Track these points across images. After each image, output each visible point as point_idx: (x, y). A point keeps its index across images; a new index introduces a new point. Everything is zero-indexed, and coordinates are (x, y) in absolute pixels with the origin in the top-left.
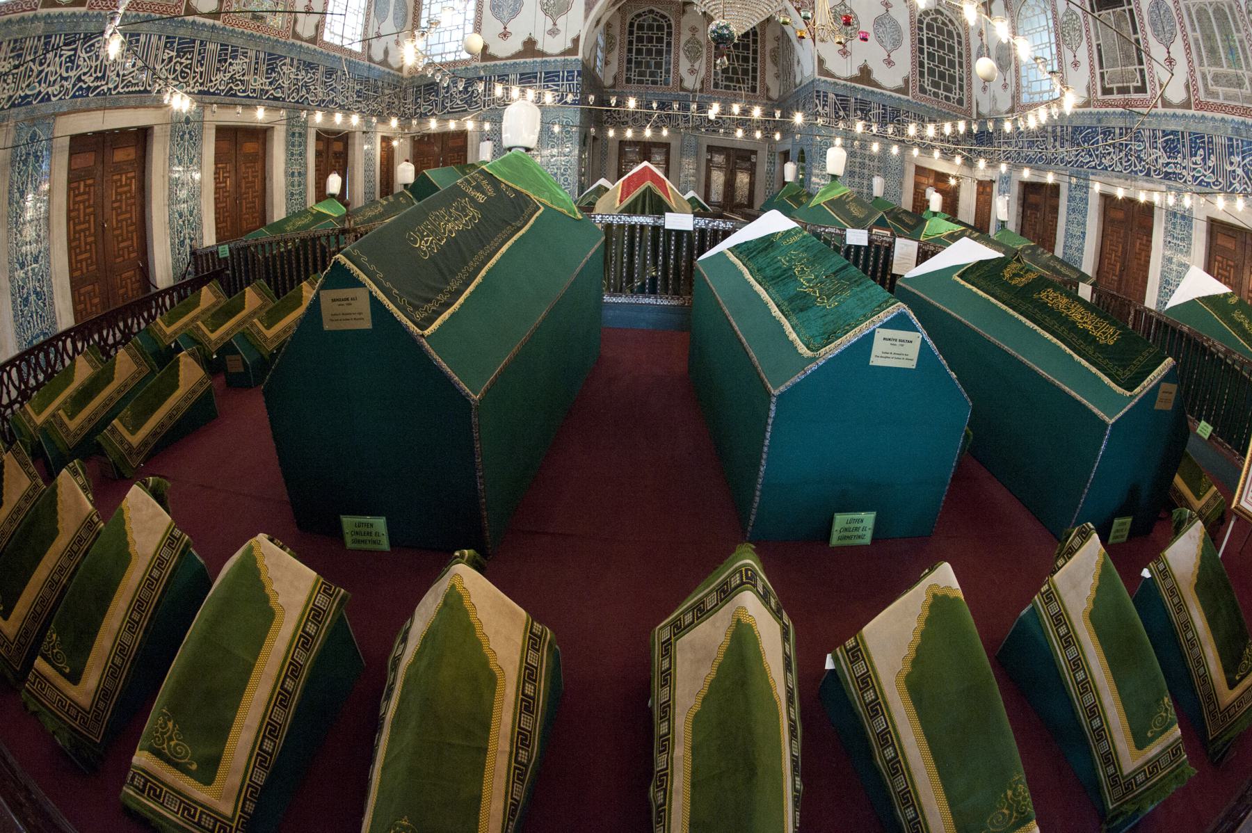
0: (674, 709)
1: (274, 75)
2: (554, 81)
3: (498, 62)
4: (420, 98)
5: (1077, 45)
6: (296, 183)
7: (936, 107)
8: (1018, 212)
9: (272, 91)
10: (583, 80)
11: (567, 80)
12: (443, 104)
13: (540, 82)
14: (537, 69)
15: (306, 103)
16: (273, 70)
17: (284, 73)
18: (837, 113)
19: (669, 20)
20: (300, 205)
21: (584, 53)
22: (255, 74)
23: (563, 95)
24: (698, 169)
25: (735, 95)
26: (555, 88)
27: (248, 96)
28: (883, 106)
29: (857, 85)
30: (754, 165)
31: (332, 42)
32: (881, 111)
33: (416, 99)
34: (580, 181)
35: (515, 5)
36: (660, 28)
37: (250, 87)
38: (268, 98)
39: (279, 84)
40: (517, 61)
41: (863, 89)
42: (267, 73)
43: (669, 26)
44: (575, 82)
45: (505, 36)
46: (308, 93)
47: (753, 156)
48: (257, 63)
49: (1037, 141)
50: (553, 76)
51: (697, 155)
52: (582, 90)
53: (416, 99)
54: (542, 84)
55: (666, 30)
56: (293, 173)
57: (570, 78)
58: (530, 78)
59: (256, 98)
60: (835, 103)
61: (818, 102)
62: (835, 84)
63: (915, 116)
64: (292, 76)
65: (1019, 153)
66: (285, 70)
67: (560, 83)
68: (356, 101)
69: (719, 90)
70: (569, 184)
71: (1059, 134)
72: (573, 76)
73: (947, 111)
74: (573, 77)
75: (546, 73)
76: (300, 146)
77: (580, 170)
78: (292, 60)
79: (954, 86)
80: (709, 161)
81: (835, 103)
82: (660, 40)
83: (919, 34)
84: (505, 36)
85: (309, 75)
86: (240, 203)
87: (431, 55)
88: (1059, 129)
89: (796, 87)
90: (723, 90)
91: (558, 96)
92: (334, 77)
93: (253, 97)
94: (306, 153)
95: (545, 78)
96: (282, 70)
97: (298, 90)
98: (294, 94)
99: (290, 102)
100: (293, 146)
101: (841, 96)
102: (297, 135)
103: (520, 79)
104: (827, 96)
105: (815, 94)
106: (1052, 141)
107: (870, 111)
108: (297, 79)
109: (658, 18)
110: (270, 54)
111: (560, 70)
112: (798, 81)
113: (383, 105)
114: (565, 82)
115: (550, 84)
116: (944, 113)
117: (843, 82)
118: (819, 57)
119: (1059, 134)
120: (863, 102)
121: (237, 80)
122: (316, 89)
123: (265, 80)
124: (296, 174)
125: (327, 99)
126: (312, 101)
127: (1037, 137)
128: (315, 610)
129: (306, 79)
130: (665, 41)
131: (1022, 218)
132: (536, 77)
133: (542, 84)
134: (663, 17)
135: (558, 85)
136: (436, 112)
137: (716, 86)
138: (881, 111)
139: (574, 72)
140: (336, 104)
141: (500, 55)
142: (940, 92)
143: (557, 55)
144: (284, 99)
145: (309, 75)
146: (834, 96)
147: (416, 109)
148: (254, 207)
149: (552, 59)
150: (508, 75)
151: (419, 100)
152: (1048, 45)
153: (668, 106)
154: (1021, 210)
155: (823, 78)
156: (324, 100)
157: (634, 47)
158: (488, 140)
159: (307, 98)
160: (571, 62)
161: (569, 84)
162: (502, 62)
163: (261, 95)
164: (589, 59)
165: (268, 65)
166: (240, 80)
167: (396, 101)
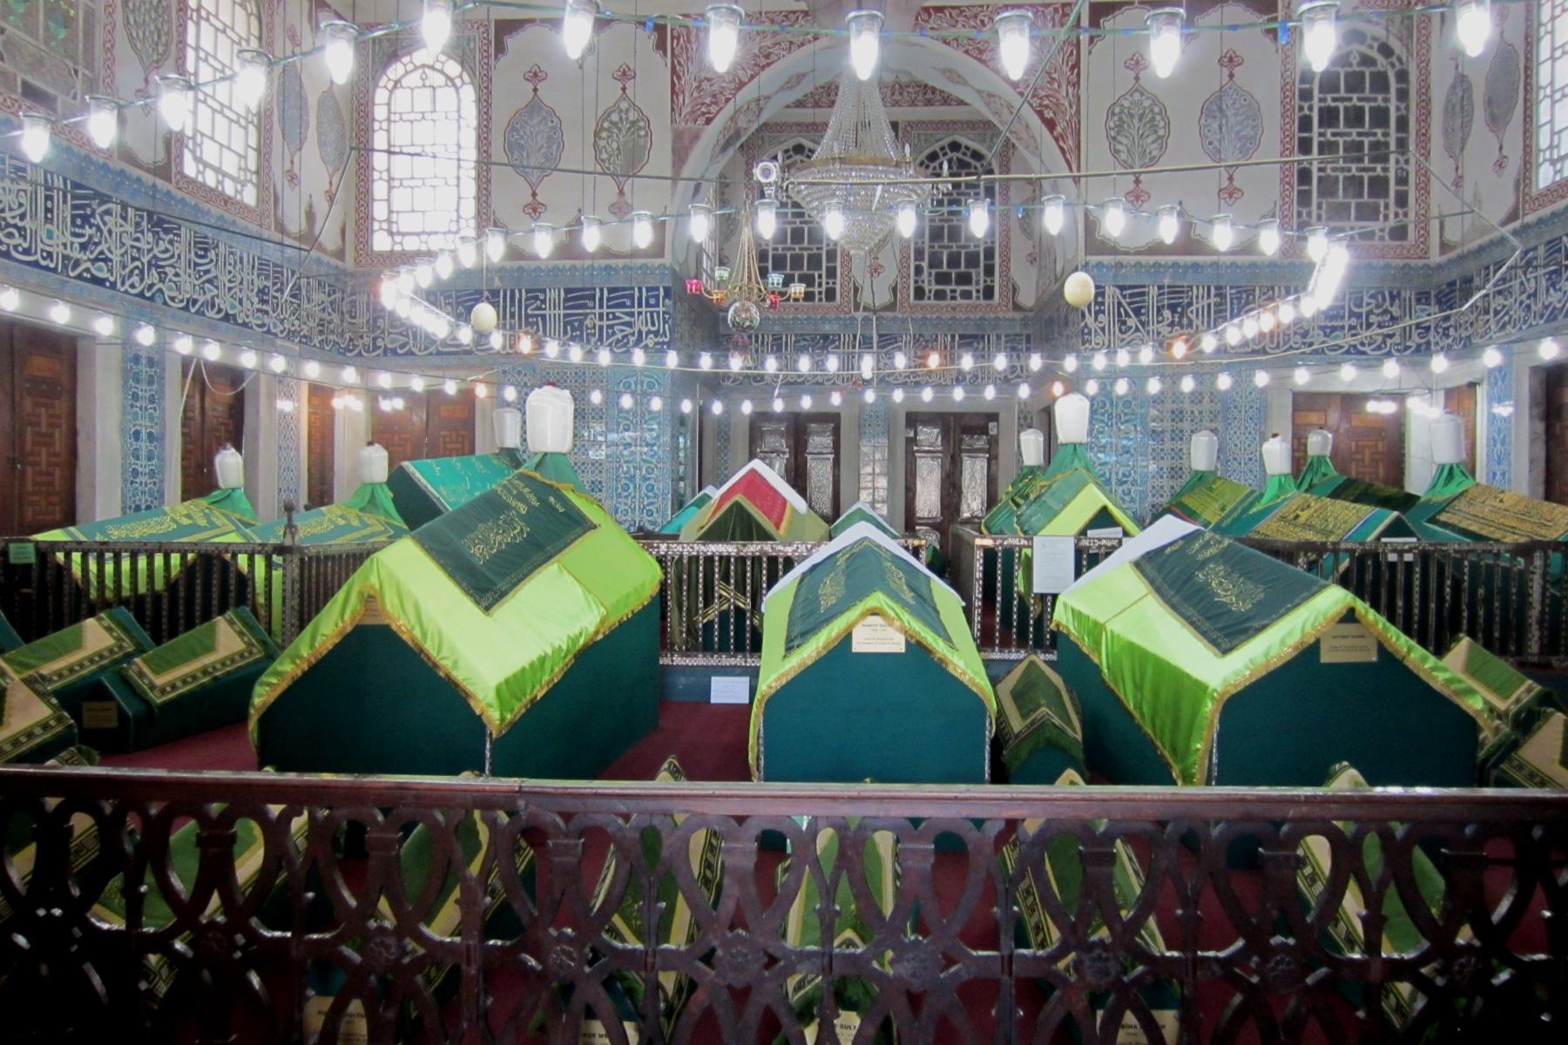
1: (88, 231)
2: (623, 305)
6: (143, 454)
8: (1533, 432)
9: (88, 265)
10: (675, 303)
11: (648, 305)
13: (601, 307)
15: (159, 301)
16: (86, 219)
17: (110, 232)
20: (151, 495)
21: (673, 252)
22: (48, 220)
24: (891, 458)
25: (954, 309)
26: (627, 319)
27: (36, 264)
30: (993, 442)
34: (675, 491)
35: (549, 147)
37: (40, 246)
38: (79, 277)
39: (102, 253)
42: (74, 224)
44: (661, 309)
45: (535, 210)
46: (162, 281)
47: (991, 425)
48: (48, 198)
50: (623, 297)
51: (890, 434)
52: (674, 323)
54: (605, 310)
56: (137, 435)
57: (652, 301)
58: (581, 298)
59: (54, 270)
64: (128, 242)
65: (1529, 307)
66: (111, 224)
67: (636, 310)
68: (259, 310)
69: (925, 302)
70: (656, 496)
72: (657, 297)
74: (658, 300)
75: (611, 291)
76: (151, 382)
77: (675, 471)
78: (124, 207)
79: (1382, 202)
80: (911, 442)
83: (1301, 109)
85: (162, 246)
86: (23, 472)
87: (399, 233)
90: (933, 302)
92: (212, 254)
93: (47, 268)
94: (162, 397)
95: (609, 300)
96: (105, 223)
97: (142, 272)
98: (135, 279)
99: (126, 292)
100: (138, 381)
102: (144, 361)
103: (566, 300)
107: (1190, 304)
108: (139, 249)
110: (76, 186)
111: (634, 284)
113: (312, 324)
115: (618, 312)
120: (1175, 291)
121: (8, 225)
122: (177, 275)
124: (144, 436)
125: (202, 299)
126: (172, 299)
129: (156, 251)
131: (1548, 442)
132: (593, 298)
133: (605, 310)
135: (632, 315)
137: (920, 293)
139: (657, 289)
140: (220, 311)
144: (113, 286)
145: (162, 246)
148: (52, 484)
150: (544, 291)
153: (833, 342)
154: (1540, 427)
156: (195, 302)
159: (160, 290)
161: (652, 313)
163: (65, 267)
164: (686, 260)
165: (75, 207)
166: (15, 226)
167: (335, 317)
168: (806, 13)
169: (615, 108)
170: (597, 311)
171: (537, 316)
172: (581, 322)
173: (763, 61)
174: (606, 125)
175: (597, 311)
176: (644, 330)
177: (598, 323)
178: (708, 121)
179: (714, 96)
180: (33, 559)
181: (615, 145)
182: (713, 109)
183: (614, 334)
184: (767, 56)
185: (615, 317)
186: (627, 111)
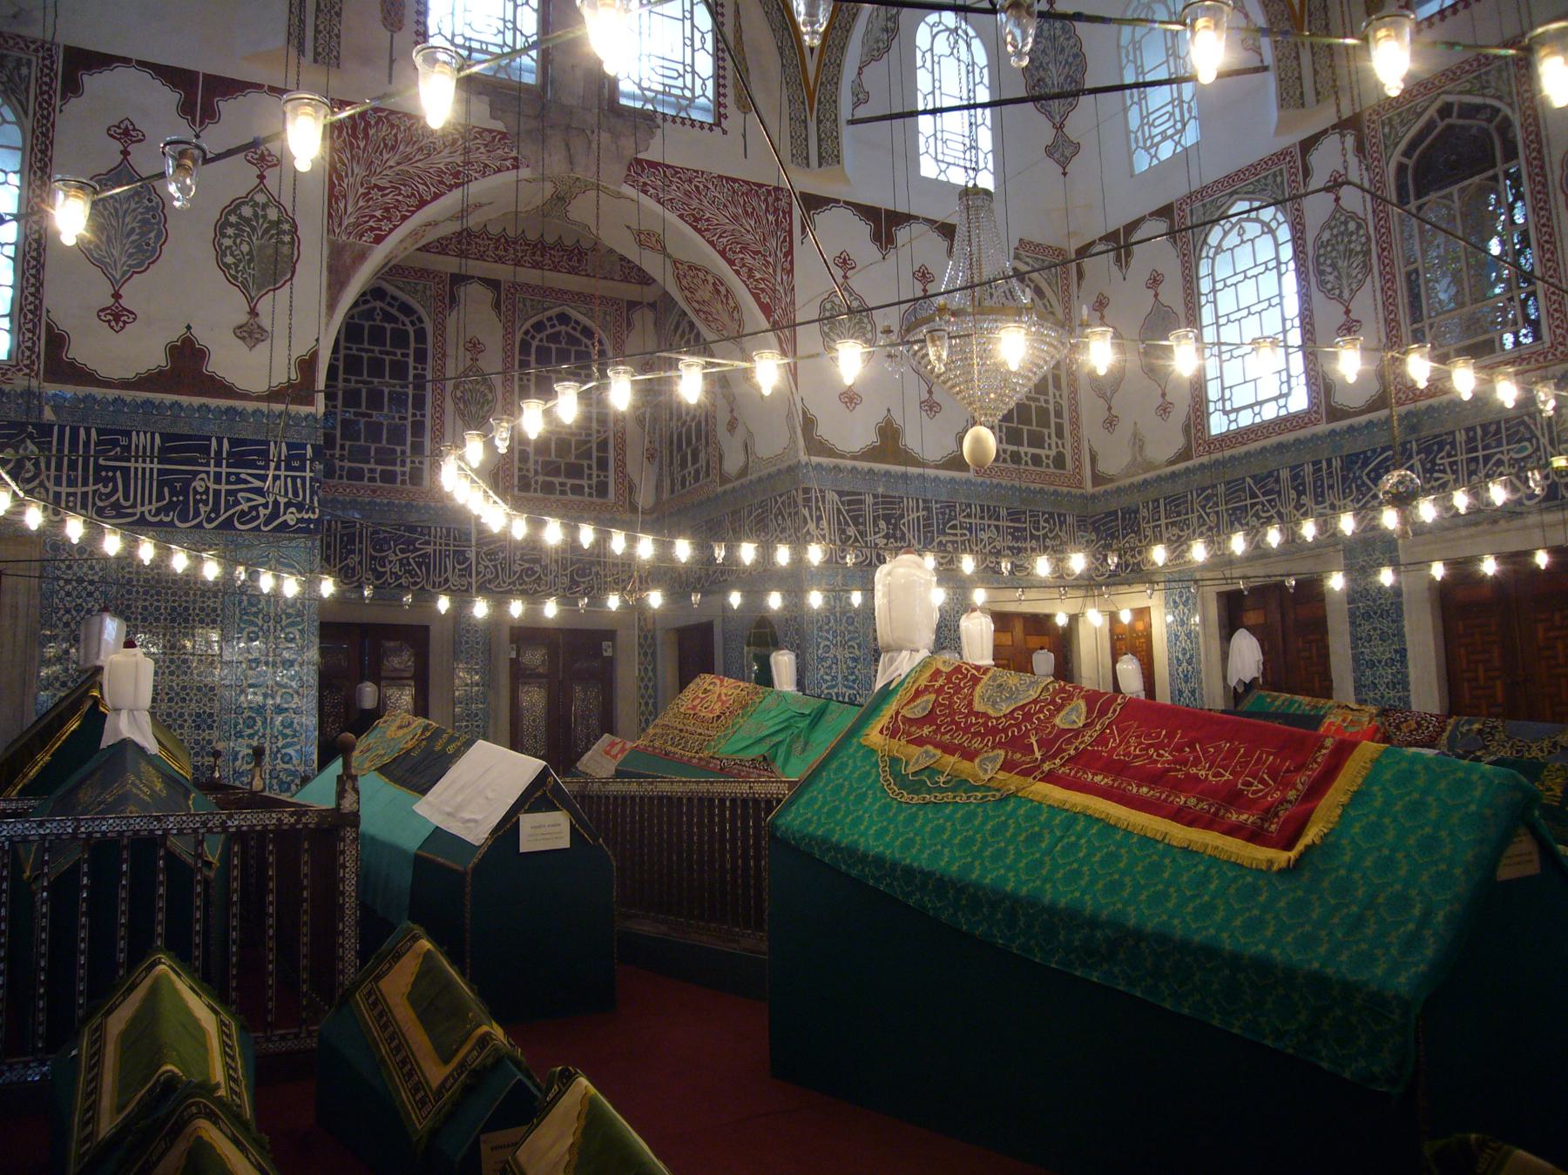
2: (253, 465)
3: (98, 392)
5: (1354, 286)
7: (1017, 483)
13: (218, 464)
14: (211, 428)
18: (843, 532)
19: (420, 320)
23: (276, 503)
26: (257, 484)
28: (925, 501)
29: (877, 466)
32: (921, 513)
36: (400, 339)
40: (157, 397)
41: (887, 473)
43: (421, 335)
44: (308, 474)
49: (1253, 505)
54: (224, 470)
55: (412, 345)
60: (839, 510)
61: (806, 512)
62: (837, 468)
63: (982, 511)
71: (1309, 480)
72: (302, 458)
73: (1038, 486)
75: (233, 443)
79: (1046, 431)
81: (839, 510)
82: (399, 370)
84: (117, 318)
88: (1309, 469)
89: (724, 479)
91: (265, 506)
101: (849, 494)
103: (163, 449)
105: (801, 496)
106: (1293, 495)
107: (902, 516)
109: (394, 312)
114: (282, 473)
115: (244, 473)
116: (1035, 492)
117: (849, 463)
118: (804, 413)
119: (1309, 480)
123: (401, 556)
127: (1253, 496)
130: (411, 372)
132: (206, 450)
134: (406, 309)
135: (263, 478)
138: (921, 513)
141: (104, 371)
142: (1022, 450)
143: (259, 398)
146: (836, 497)
149: (250, 406)
150: (128, 434)
152: (1222, 321)
155: (815, 459)
157: (341, 384)
160: (297, 419)
161: (294, 479)
162: (111, 394)
168: (504, 136)
169: (248, 199)
170: (212, 469)
171: (114, 469)
173: (449, 180)
174: (233, 219)
175: (212, 469)
176: (282, 500)
177: (212, 486)
178: (379, 240)
179: (387, 210)
181: (245, 248)
182: (386, 225)
183: (237, 503)
184: (456, 175)
185: (240, 481)
186: (265, 206)
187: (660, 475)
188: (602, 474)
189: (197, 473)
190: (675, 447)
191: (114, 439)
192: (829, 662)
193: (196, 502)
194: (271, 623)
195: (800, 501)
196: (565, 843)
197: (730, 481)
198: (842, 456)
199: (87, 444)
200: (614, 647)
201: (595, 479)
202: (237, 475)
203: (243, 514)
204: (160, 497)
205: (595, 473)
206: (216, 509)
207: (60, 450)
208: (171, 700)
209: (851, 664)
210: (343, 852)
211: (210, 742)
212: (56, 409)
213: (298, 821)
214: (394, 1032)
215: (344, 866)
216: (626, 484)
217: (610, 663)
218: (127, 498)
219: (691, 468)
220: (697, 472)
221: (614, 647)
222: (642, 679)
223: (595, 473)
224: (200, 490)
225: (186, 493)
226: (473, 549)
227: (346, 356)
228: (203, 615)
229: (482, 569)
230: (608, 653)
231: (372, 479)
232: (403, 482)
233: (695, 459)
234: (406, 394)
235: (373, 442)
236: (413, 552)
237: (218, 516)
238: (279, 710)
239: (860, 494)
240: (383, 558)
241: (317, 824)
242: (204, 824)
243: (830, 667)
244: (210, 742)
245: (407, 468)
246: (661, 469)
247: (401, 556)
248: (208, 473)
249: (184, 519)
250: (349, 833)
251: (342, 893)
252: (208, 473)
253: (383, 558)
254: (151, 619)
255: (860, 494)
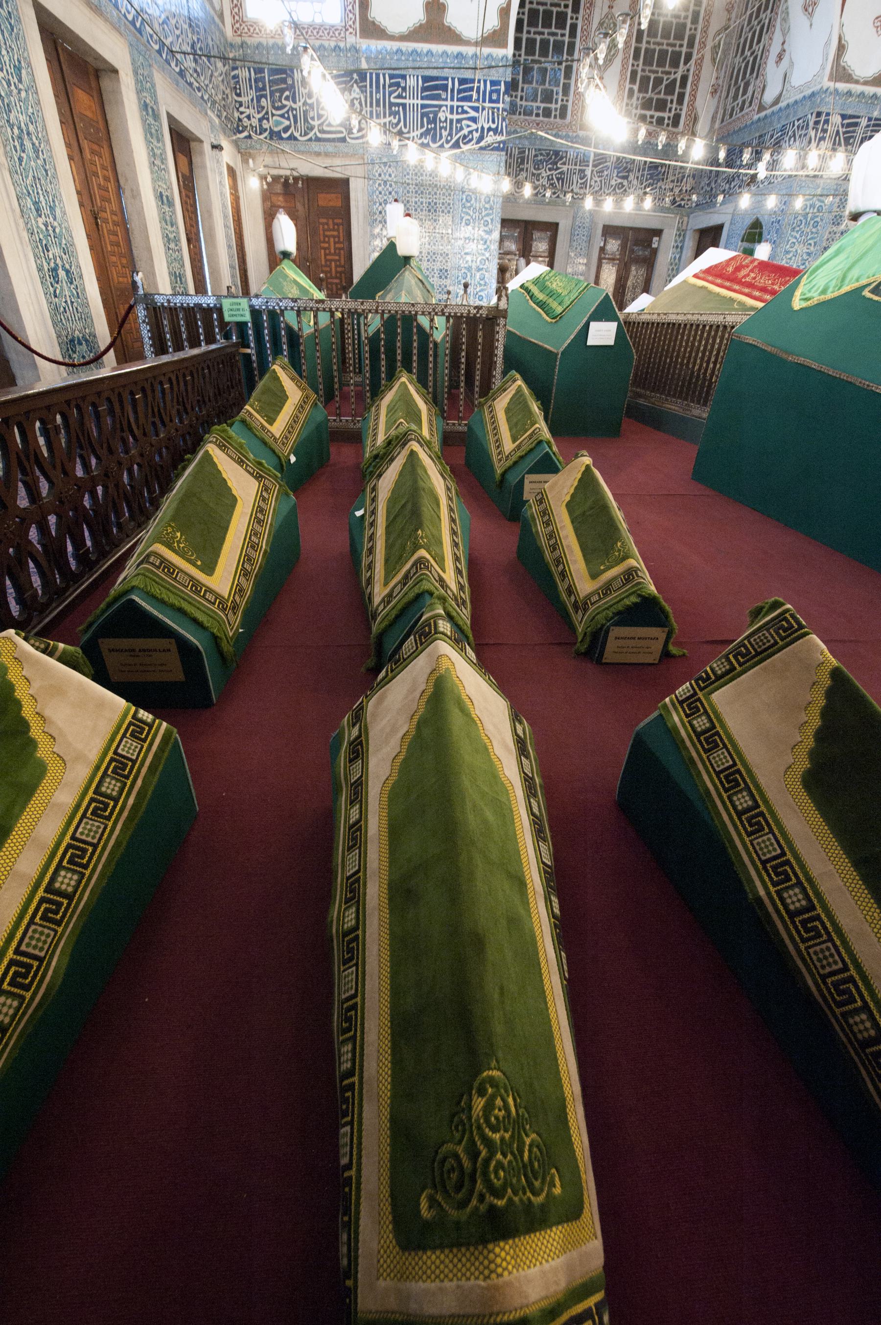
0: (366, 832)
4: (265, 96)
11: (491, 101)
12: (306, 120)
13: (452, 100)
26: (473, 114)
31: (318, 20)
33: (259, 101)
53: (259, 101)
61: (813, 133)
72: (498, 91)
89: (761, 108)
95: (459, 92)
103: (424, 89)
104: (827, 122)
112: (769, 97)
115: (466, 105)
118: (840, 39)
123: (549, 173)
128: (134, 725)
132: (445, 88)
135: (476, 109)
136: (297, 135)
147: (260, 120)
150: (404, 77)
151: (263, 102)
158: (396, 200)
171: (398, 105)
172: (436, 114)
177: (449, 116)
180: (247, 318)
183: (462, 129)
187: (718, 107)
188: (679, 108)
189: (440, 106)
190: (733, 82)
191: (397, 80)
192: (791, 255)
193: (441, 128)
194: (477, 214)
195: (811, 124)
196: (612, 343)
197: (765, 109)
198: (857, 82)
199: (384, 85)
200: (659, 241)
201: (673, 112)
202: (462, 107)
203: (465, 137)
204: (422, 126)
205: (674, 106)
206: (450, 134)
207: (371, 93)
208: (428, 260)
209: (805, 257)
210: (498, 332)
211: (446, 286)
212: (368, 59)
213: (478, 312)
214: (553, 531)
215: (498, 340)
216: (693, 116)
217: (655, 252)
218: (405, 127)
219: (740, 100)
220: (744, 102)
221: (659, 241)
222: (671, 264)
223: (674, 106)
224: (443, 119)
225: (434, 121)
226: (590, 168)
227: (530, 10)
228: (443, 207)
229: (593, 183)
230: (654, 246)
231: (538, 115)
232: (555, 117)
233: (745, 92)
234: (563, 42)
235: (541, 84)
236: (556, 170)
237: (452, 139)
238: (479, 270)
239: (858, 117)
240: (539, 175)
241: (487, 315)
242: (434, 310)
243: (790, 259)
244: (446, 286)
245: (559, 106)
246: (719, 102)
247: (549, 173)
248: (446, 106)
249: (434, 141)
250: (502, 321)
251: (496, 355)
252: (446, 106)
253: (539, 175)
254: (419, 210)
255: (858, 117)
